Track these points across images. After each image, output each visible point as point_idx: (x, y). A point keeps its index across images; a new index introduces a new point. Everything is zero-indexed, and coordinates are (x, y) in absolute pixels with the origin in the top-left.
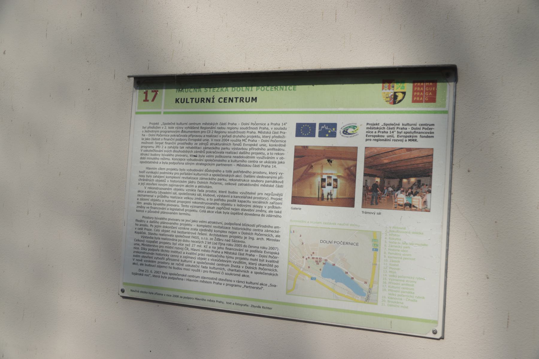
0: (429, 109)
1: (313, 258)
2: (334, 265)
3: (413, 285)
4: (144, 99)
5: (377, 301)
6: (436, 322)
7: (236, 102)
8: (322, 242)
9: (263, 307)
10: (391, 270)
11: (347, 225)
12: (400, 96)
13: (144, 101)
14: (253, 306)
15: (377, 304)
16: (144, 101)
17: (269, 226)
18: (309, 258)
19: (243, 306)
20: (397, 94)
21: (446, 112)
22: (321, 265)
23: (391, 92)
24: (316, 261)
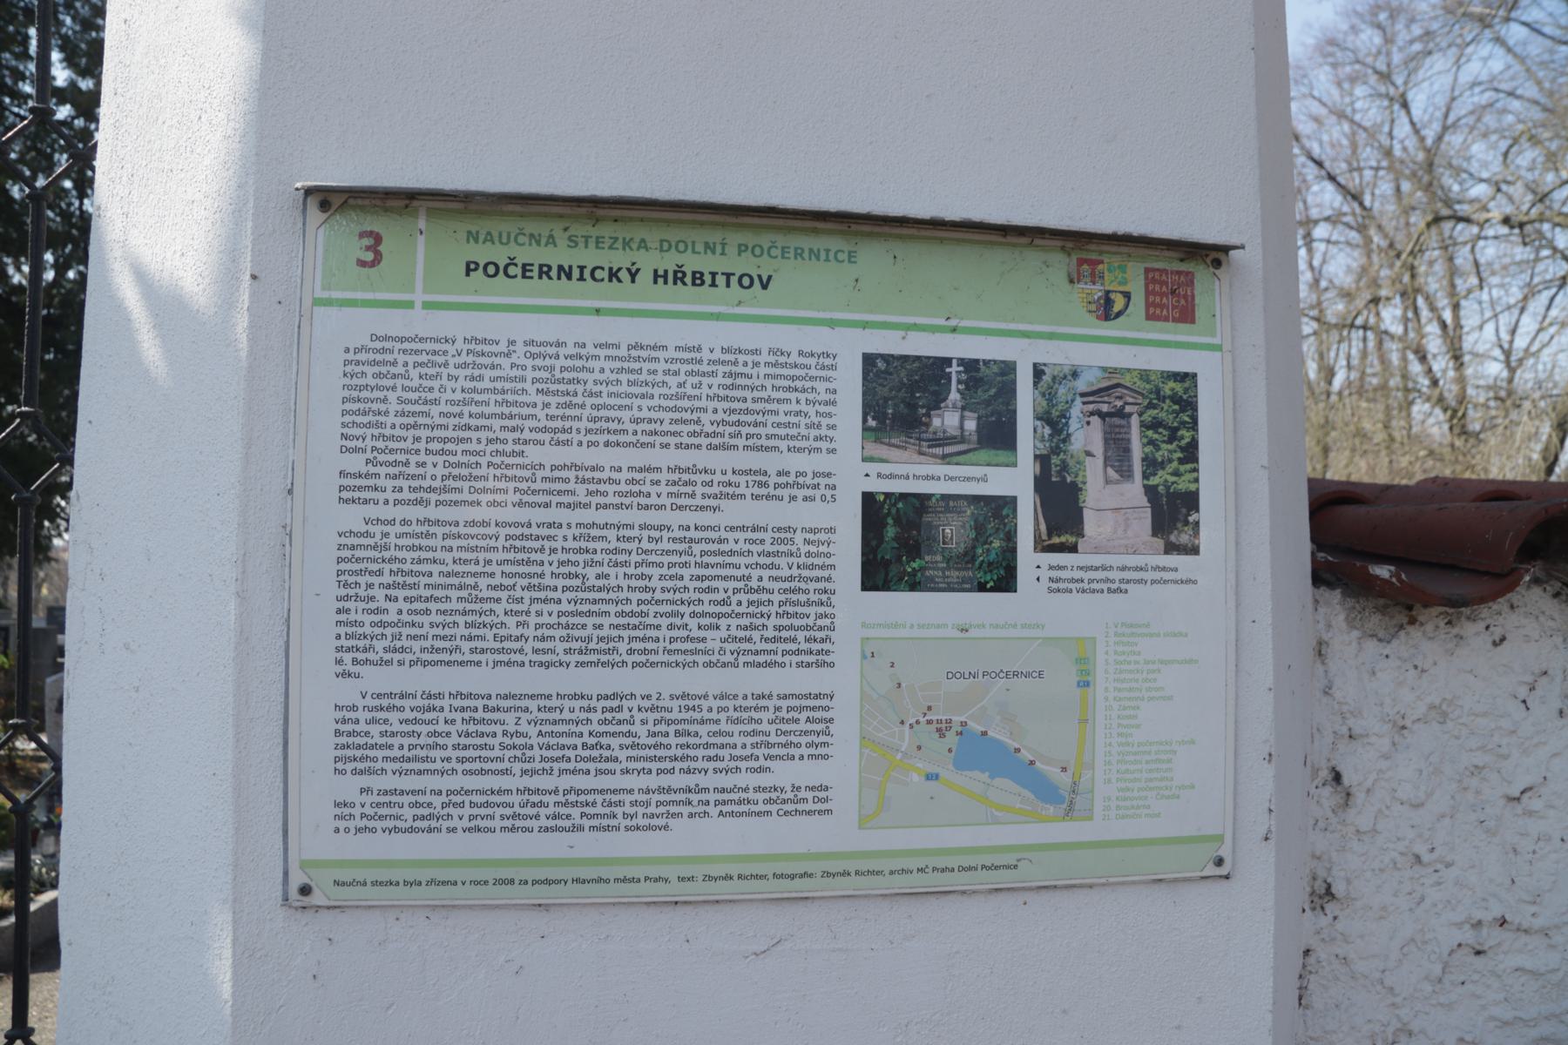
1: (929, 722)
2: (984, 734)
3: (1170, 761)
5: (1091, 810)
6: (1220, 839)
7: (728, 285)
8: (951, 675)
9: (857, 873)
10: (1121, 730)
11: (1015, 626)
14: (708, 878)
15: (1091, 819)
18: (918, 722)
19: (797, 880)
20: (1113, 296)
21: (1218, 348)
22: (951, 739)
23: (1097, 291)
24: (939, 730)
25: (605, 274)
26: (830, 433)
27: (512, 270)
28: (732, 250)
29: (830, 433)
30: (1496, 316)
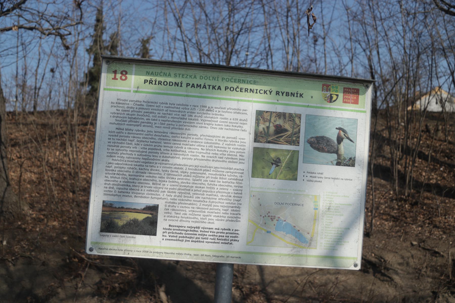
0: (353, 109)
1: (269, 216)
4: (113, 77)
12: (335, 97)
13: (113, 79)
16: (113, 79)
17: (224, 243)
21: (365, 112)
23: (328, 94)
24: (271, 219)
25: (263, 92)
26: (110, 137)
27: (237, 89)
28: (220, 79)
29: (110, 137)
30: (33, 58)
